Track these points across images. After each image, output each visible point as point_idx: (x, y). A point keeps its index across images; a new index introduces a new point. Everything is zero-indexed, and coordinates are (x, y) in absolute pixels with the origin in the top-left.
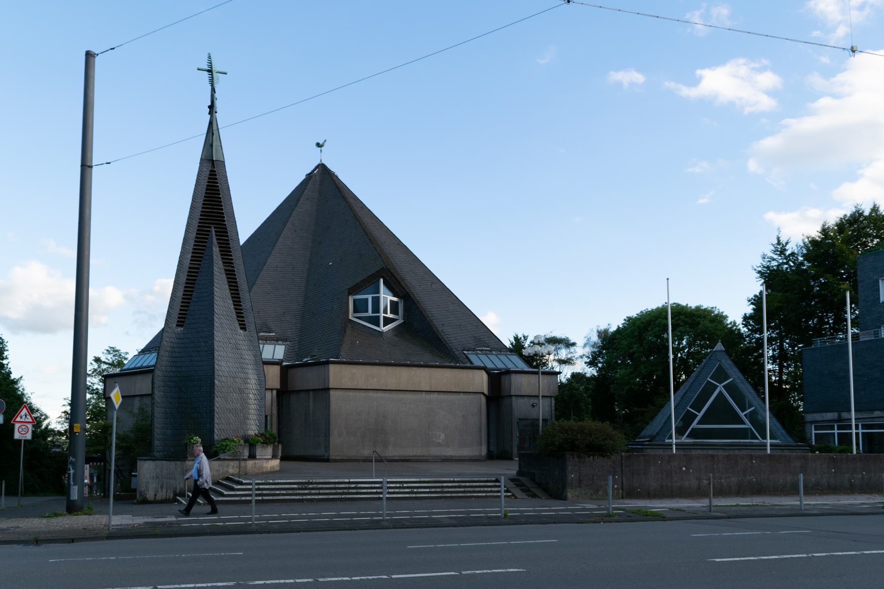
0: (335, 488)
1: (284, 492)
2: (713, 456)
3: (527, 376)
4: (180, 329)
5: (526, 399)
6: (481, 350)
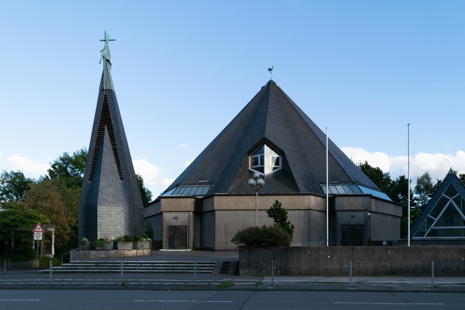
0: (188, 266)
1: (82, 268)
2: (436, 249)
3: (347, 198)
4: (90, 182)
5: (347, 212)
6: (332, 183)
